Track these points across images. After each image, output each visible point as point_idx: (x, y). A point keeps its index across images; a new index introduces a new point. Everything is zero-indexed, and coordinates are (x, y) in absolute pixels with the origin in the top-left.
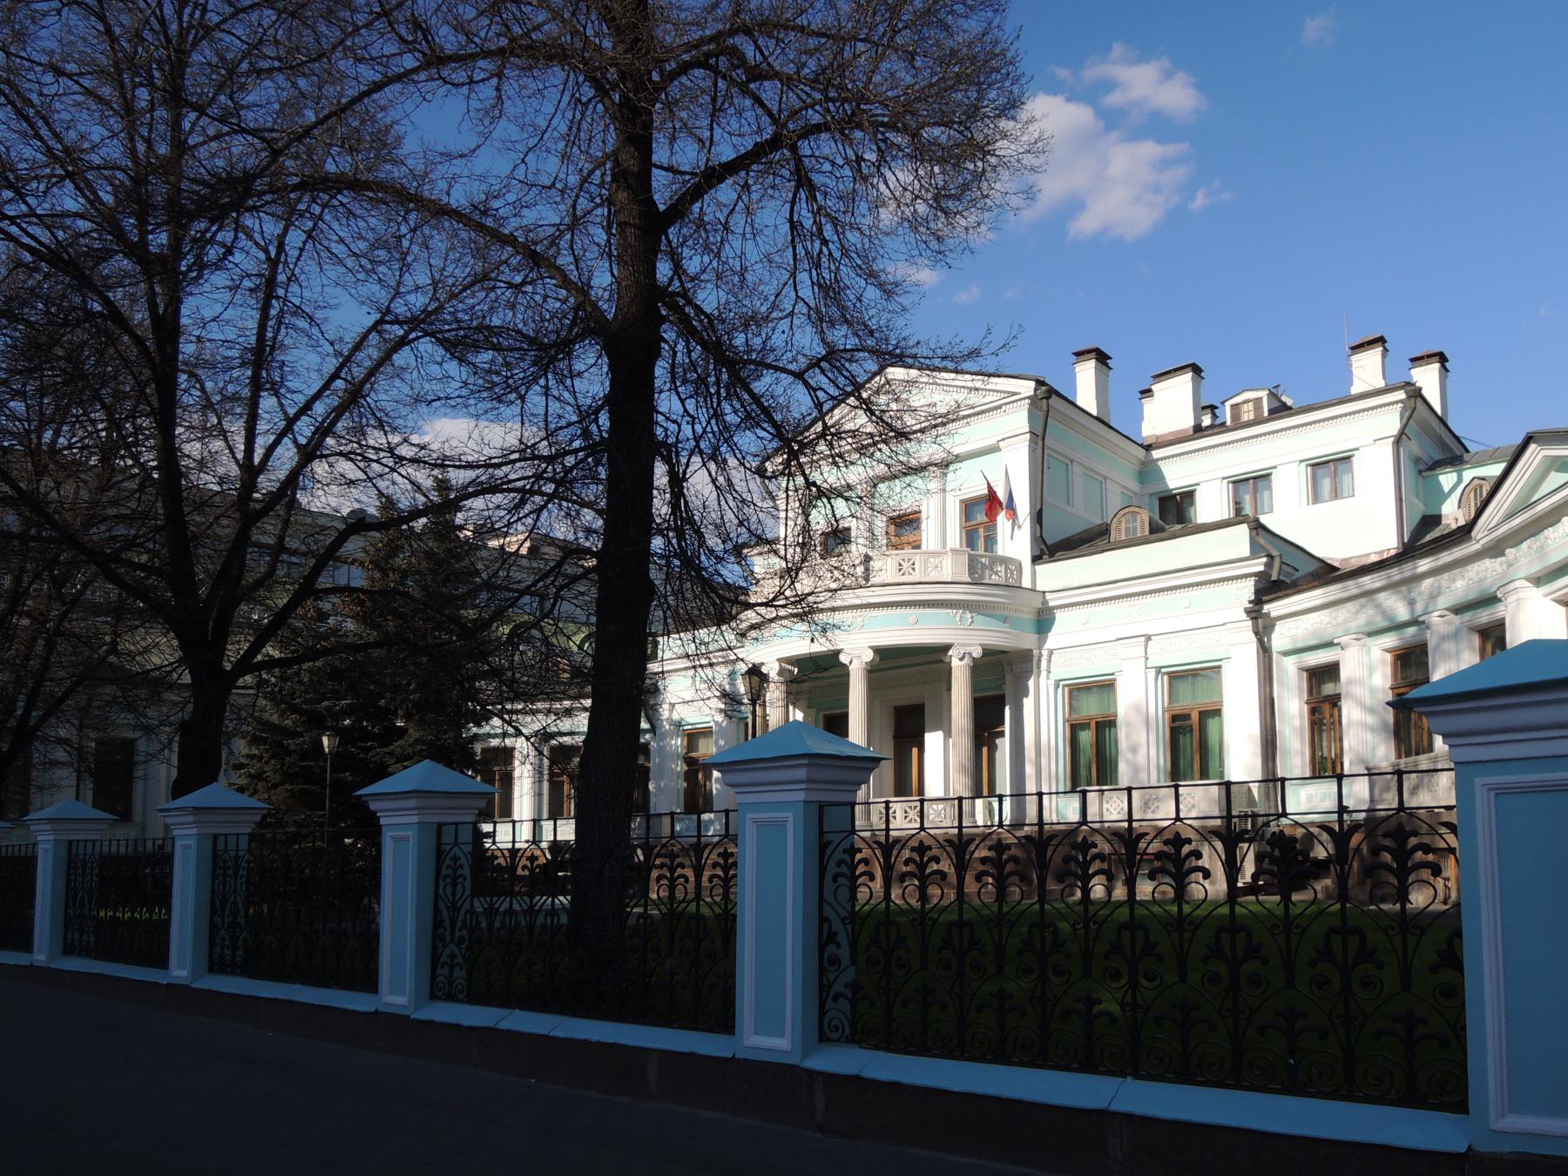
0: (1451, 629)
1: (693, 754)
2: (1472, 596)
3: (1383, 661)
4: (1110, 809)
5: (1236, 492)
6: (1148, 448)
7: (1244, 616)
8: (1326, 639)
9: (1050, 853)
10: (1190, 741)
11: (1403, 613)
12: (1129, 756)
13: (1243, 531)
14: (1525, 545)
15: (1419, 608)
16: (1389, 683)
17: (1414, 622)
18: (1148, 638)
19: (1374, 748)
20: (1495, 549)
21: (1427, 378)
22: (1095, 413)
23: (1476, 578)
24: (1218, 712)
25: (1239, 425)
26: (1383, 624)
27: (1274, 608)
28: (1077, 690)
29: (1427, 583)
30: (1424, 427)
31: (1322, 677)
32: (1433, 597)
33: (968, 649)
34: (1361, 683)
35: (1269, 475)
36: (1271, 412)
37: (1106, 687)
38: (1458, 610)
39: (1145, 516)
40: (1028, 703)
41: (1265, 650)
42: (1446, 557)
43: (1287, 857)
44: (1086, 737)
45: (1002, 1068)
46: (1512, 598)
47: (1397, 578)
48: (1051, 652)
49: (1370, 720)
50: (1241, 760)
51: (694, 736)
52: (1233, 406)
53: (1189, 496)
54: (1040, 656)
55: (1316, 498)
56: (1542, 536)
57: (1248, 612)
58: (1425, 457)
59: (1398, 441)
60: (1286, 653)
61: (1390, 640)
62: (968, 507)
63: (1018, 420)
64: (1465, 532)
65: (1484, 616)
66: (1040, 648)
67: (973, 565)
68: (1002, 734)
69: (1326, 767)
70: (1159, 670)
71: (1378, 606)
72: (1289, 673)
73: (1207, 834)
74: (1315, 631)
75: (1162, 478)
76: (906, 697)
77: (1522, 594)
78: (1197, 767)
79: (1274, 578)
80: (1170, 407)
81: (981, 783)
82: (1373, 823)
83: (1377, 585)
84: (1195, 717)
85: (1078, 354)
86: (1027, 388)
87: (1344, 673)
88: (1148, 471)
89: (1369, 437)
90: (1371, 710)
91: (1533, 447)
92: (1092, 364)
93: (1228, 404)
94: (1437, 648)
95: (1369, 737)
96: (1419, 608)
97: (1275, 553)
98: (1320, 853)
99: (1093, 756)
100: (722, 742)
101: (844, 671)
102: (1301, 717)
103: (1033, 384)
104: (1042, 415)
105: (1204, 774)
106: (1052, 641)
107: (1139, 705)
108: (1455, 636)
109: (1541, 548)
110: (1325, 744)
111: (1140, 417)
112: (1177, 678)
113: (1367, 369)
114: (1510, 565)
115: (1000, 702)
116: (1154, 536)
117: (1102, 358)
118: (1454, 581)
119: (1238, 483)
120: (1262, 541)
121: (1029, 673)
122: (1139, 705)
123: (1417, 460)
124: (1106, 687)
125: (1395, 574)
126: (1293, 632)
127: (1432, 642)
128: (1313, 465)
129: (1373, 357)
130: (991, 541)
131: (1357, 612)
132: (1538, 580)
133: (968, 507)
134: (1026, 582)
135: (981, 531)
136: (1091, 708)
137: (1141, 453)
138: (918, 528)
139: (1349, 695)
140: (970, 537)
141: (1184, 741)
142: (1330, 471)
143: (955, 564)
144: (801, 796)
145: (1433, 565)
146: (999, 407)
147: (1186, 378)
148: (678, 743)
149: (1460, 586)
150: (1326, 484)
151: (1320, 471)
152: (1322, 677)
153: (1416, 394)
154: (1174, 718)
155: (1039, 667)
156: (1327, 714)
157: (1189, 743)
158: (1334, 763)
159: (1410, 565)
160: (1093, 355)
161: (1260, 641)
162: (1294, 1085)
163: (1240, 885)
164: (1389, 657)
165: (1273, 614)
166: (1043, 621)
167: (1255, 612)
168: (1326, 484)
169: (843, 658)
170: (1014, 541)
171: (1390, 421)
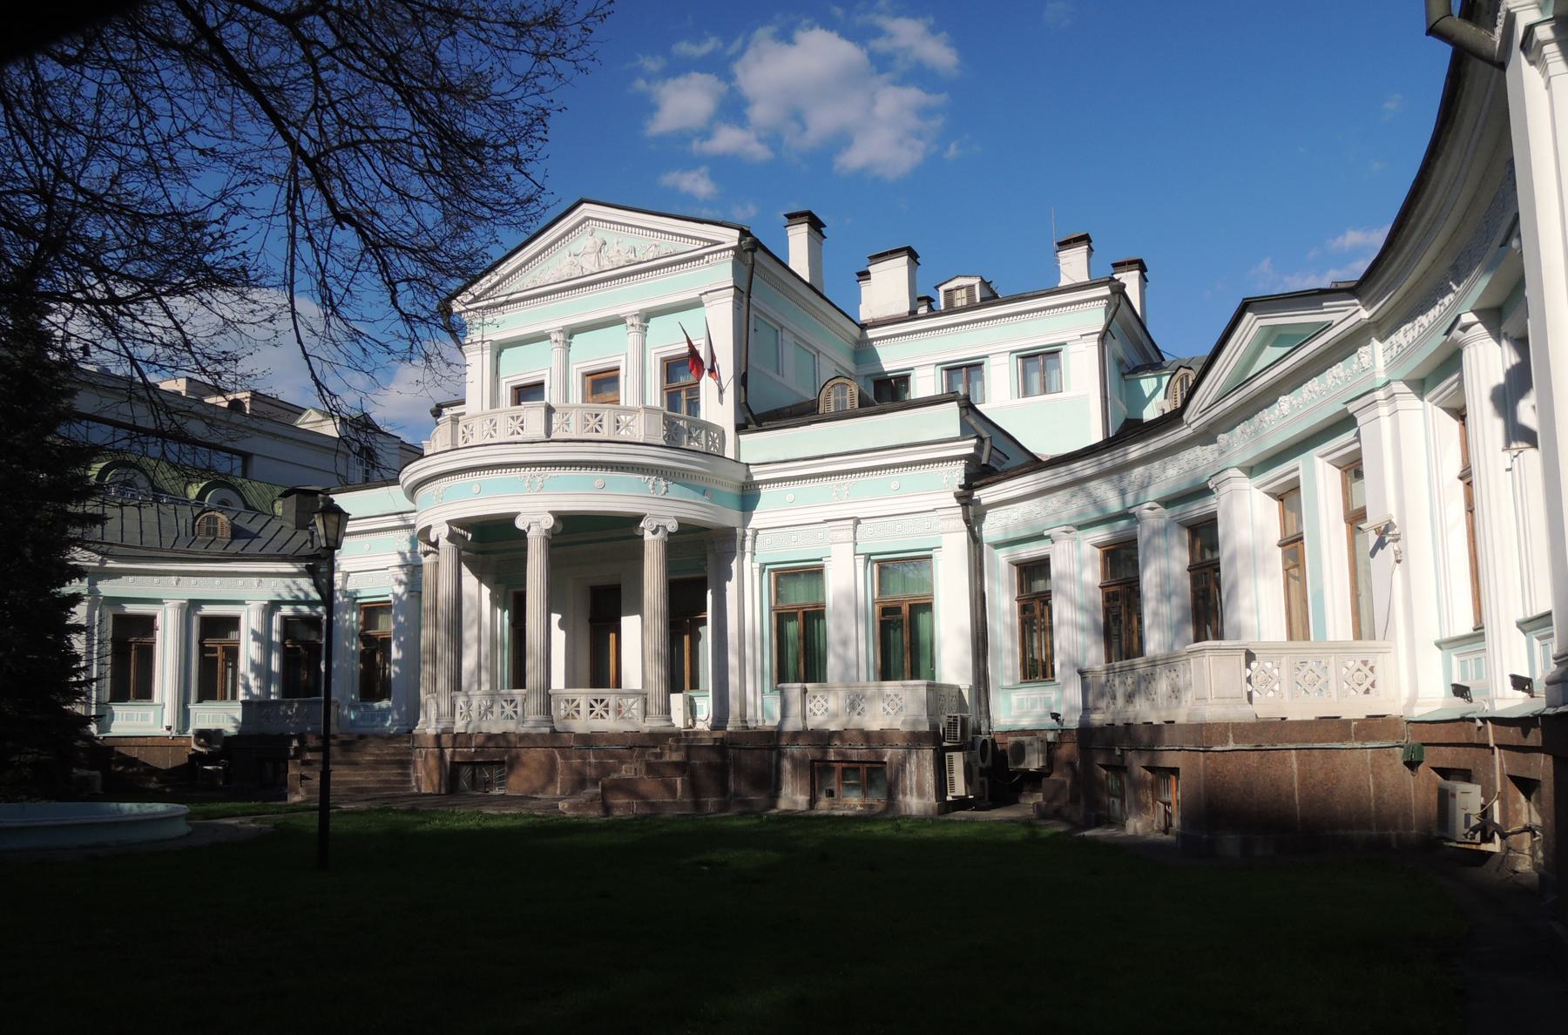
0: (1162, 522)
1: (370, 632)
2: (1184, 485)
3: (1093, 557)
4: (823, 709)
5: (949, 378)
6: (864, 327)
7: (954, 502)
8: (1037, 531)
9: (743, 757)
10: (901, 638)
11: (1114, 505)
12: (840, 650)
13: (953, 409)
14: (1238, 429)
15: (1130, 499)
16: (1098, 581)
17: (1125, 515)
18: (857, 521)
19: (1085, 650)
20: (1206, 436)
21: (1130, 280)
22: (807, 279)
23: (1186, 467)
24: (928, 607)
25: (951, 309)
26: (1094, 515)
27: (985, 495)
29: (1138, 471)
30: (1126, 328)
31: (1033, 572)
32: (1144, 487)
33: (662, 522)
34: (1072, 578)
35: (981, 364)
36: (982, 299)
38: (1168, 502)
39: (854, 389)
40: (731, 587)
41: (975, 540)
42: (1155, 444)
43: (999, 768)
44: (793, 628)
46: (1224, 489)
47: (1108, 465)
48: (756, 532)
49: (1082, 619)
50: (952, 663)
51: (372, 611)
53: (903, 380)
54: (744, 536)
55: (1026, 392)
56: (1256, 419)
57: (958, 497)
58: (1126, 359)
59: (1103, 337)
60: (997, 545)
61: (1101, 534)
62: (671, 367)
63: (721, 272)
64: (1171, 419)
65: (1196, 510)
66: (744, 526)
67: (670, 424)
68: (704, 622)
69: (1036, 669)
70: (868, 557)
71: (1089, 495)
72: (1000, 566)
73: (915, 740)
74: (1026, 521)
75: (876, 360)
76: (602, 575)
77: (1234, 485)
78: (907, 665)
79: (984, 461)
80: (886, 289)
81: (678, 674)
82: (1087, 735)
83: (1089, 472)
84: (905, 609)
85: (790, 216)
86: (731, 237)
87: (1054, 568)
88: (863, 351)
89: (1076, 330)
90: (1082, 609)
91: (1249, 315)
92: (804, 228)
93: (942, 289)
94: (1148, 542)
95: (1081, 639)
96: (1130, 499)
97: (985, 435)
98: (1034, 762)
99: (800, 649)
100: (401, 619)
102: (1012, 616)
103: (736, 233)
104: (746, 270)
105: (915, 674)
106: (758, 519)
107: (846, 586)
108: (1164, 531)
109: (1256, 431)
110: (1036, 644)
111: (858, 300)
112: (886, 567)
113: (1074, 264)
114: (1222, 452)
115: (700, 586)
116: (863, 410)
117: (816, 225)
118: (1164, 470)
119: (952, 370)
120: (972, 422)
121: (734, 554)
122: (846, 586)
123: (1120, 363)
124: (814, 573)
125: (1107, 460)
126: (1004, 522)
127: (1143, 534)
128: (1023, 357)
129: (1080, 252)
130: (694, 406)
131: (1067, 502)
132: (1251, 470)
133: (671, 367)
134: (730, 453)
135: (683, 394)
136: (798, 596)
137: (856, 331)
138: (617, 388)
139: (1059, 590)
140: (672, 399)
141: (894, 636)
142: (1039, 364)
143: (648, 423)
145: (1144, 451)
146: (702, 257)
147: (903, 260)
148: (352, 618)
149: (1171, 475)
150: (1035, 378)
151: (1030, 364)
152: (1033, 572)
153: (1119, 290)
154: (885, 611)
155: (743, 548)
156: (1037, 612)
157: (900, 638)
158: (1044, 666)
159: (1119, 452)
160: (806, 219)
161: (971, 530)
163: (949, 798)
164: (1098, 552)
165: (983, 502)
166: (748, 496)
167: (965, 497)
168: (1035, 378)
169: (520, 524)
170: (717, 406)
171: (1095, 317)
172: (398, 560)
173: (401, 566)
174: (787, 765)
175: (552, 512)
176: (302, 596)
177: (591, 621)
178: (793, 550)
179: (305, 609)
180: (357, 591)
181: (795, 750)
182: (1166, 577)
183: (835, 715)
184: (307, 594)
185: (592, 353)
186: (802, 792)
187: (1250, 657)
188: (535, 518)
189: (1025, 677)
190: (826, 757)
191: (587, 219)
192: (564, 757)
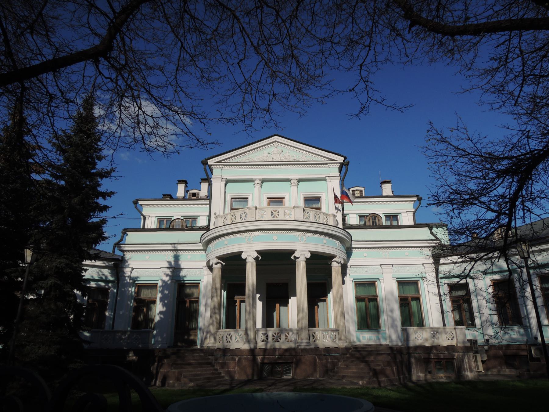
28: (359, 284)
37: (372, 284)
52: (352, 191)
63: (334, 170)
86: (340, 159)
93: (351, 190)
103: (343, 158)
107: (387, 290)
112: (402, 283)
122: (387, 290)
124: (372, 284)
146: (327, 164)
169: (243, 256)
172: (167, 265)
173: (168, 268)
174: (413, 361)
175: (256, 251)
177: (267, 298)
178: (366, 275)
179: (103, 284)
180: (138, 277)
181: (416, 354)
183: (427, 340)
184: (106, 277)
185: (275, 190)
186: (421, 372)
188: (303, 253)
189: (358, 329)
190: (431, 356)
191: (276, 141)
192: (320, 359)
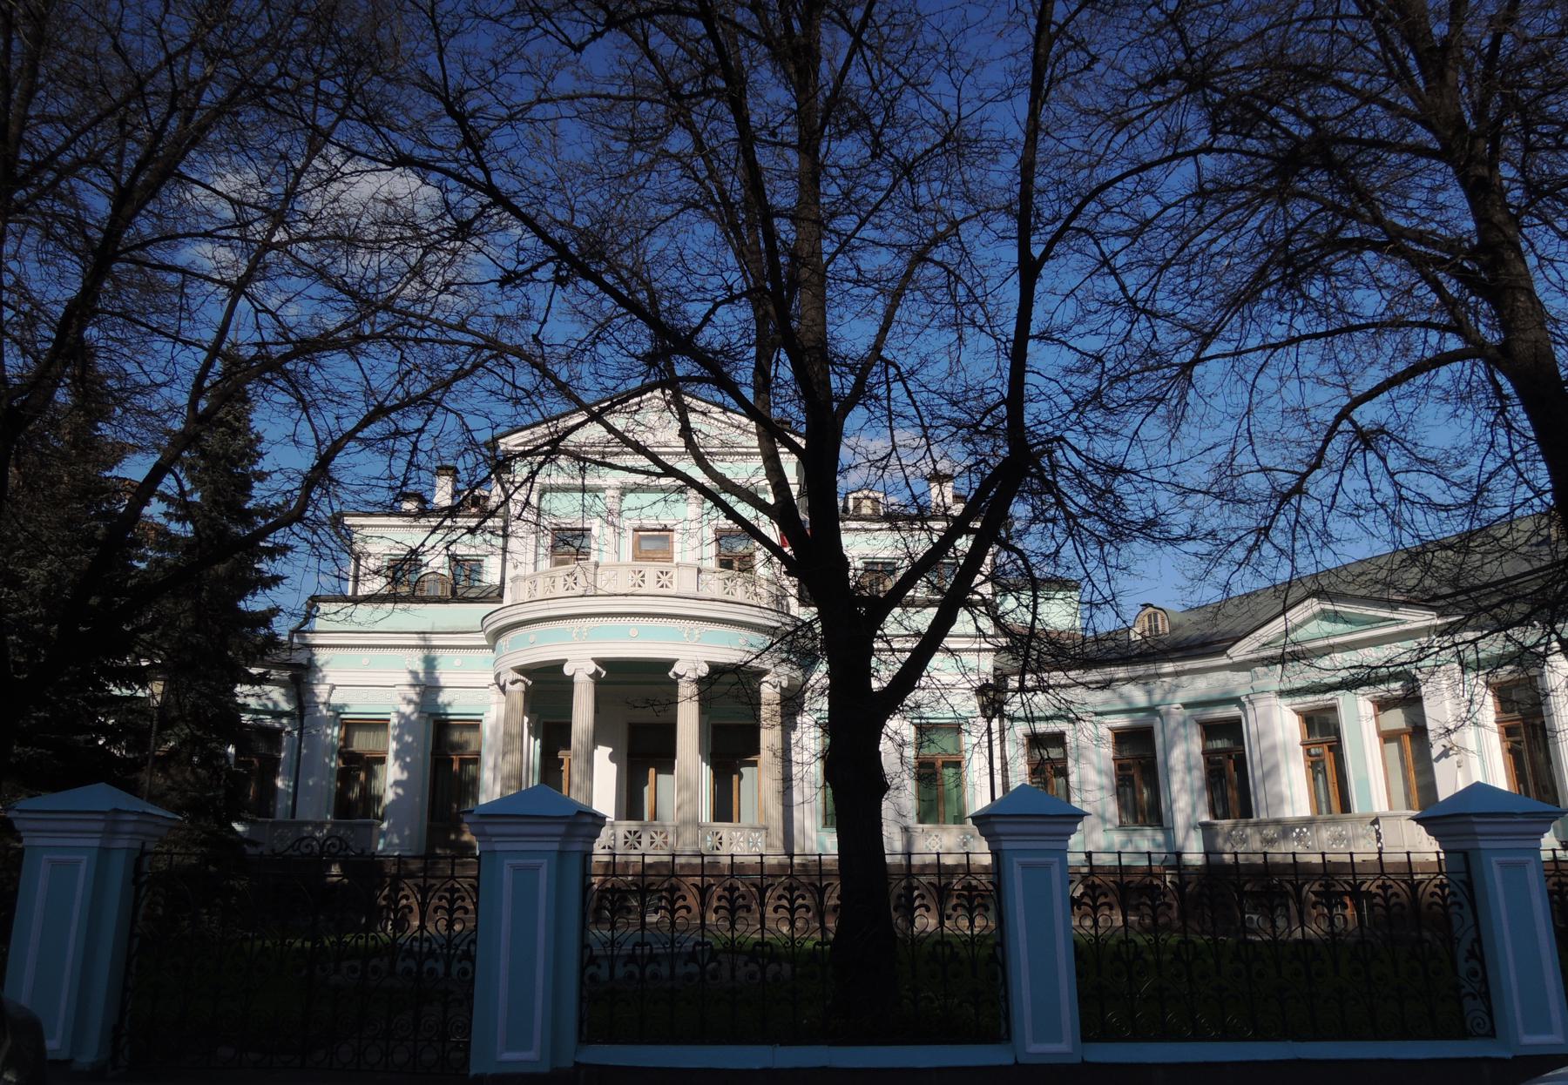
2: (1215, 695)
38: (1185, 706)
45: (1409, 1042)
90: (1100, 772)
101: (570, 681)
108: (1184, 724)
132: (1281, 694)
144: (96, 843)
162: (1405, 1035)
172: (408, 679)
176: (270, 705)
179: (268, 720)
180: (344, 706)
182: (1188, 755)
184: (276, 704)
187: (1376, 822)
